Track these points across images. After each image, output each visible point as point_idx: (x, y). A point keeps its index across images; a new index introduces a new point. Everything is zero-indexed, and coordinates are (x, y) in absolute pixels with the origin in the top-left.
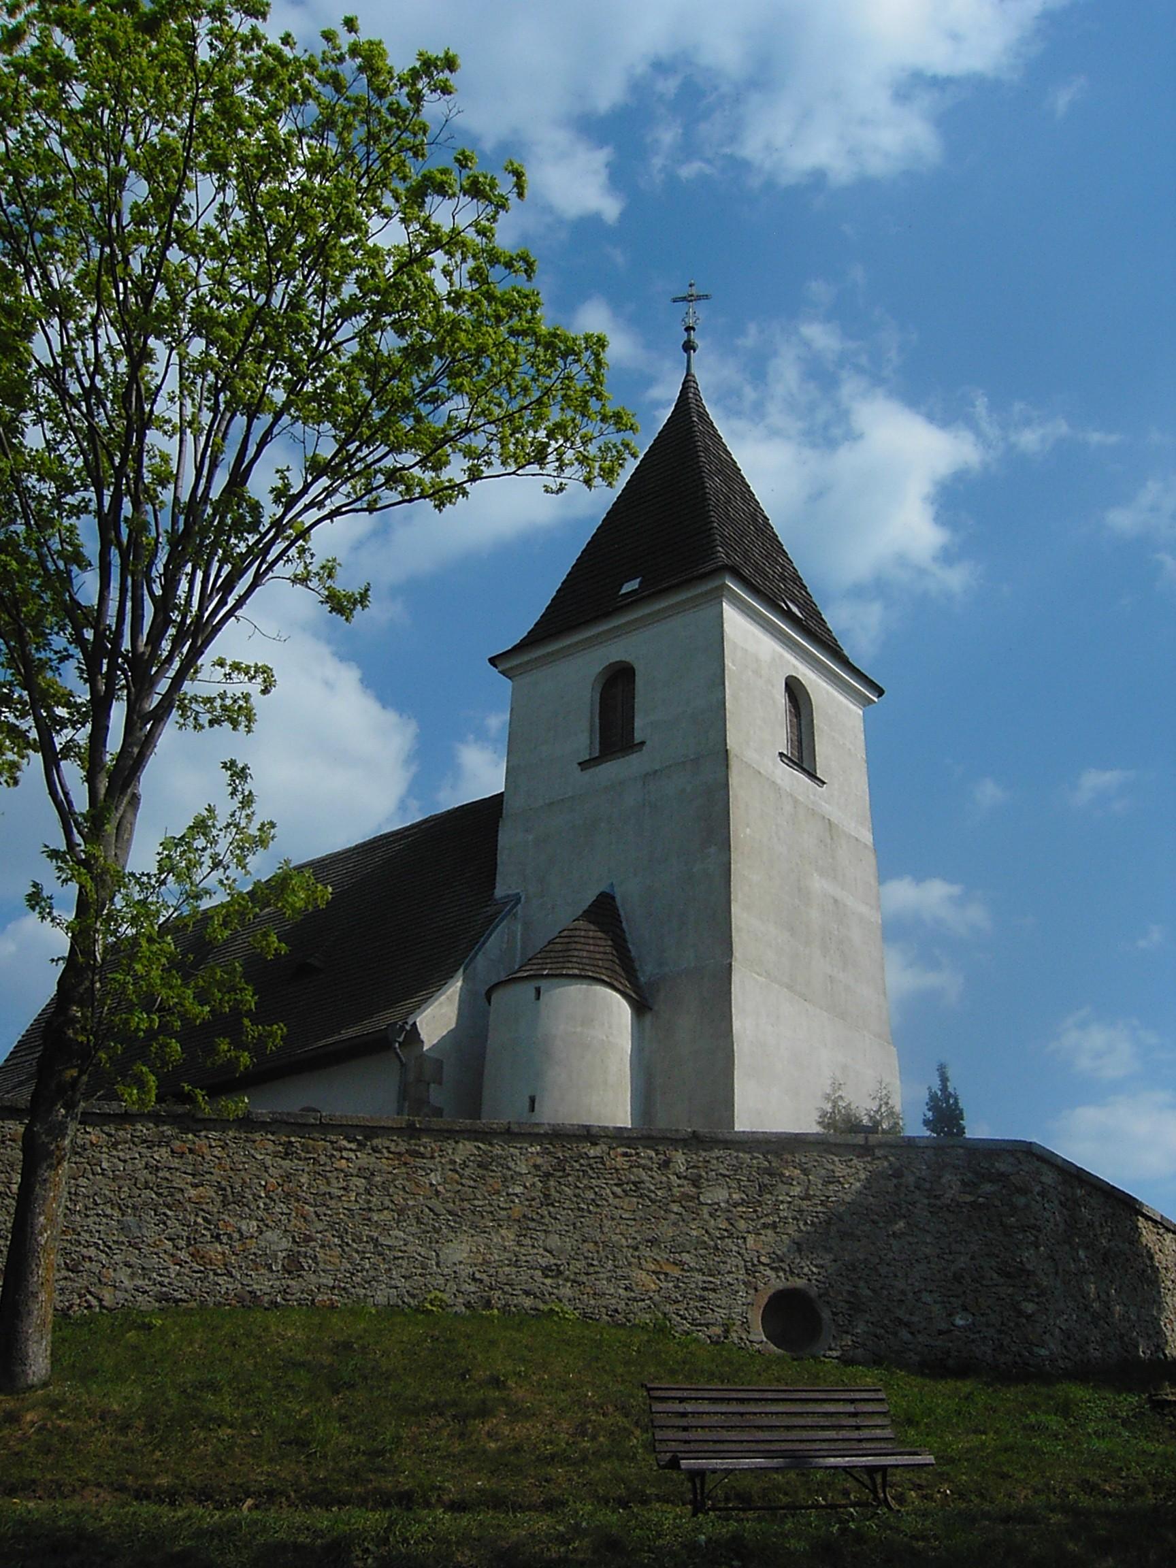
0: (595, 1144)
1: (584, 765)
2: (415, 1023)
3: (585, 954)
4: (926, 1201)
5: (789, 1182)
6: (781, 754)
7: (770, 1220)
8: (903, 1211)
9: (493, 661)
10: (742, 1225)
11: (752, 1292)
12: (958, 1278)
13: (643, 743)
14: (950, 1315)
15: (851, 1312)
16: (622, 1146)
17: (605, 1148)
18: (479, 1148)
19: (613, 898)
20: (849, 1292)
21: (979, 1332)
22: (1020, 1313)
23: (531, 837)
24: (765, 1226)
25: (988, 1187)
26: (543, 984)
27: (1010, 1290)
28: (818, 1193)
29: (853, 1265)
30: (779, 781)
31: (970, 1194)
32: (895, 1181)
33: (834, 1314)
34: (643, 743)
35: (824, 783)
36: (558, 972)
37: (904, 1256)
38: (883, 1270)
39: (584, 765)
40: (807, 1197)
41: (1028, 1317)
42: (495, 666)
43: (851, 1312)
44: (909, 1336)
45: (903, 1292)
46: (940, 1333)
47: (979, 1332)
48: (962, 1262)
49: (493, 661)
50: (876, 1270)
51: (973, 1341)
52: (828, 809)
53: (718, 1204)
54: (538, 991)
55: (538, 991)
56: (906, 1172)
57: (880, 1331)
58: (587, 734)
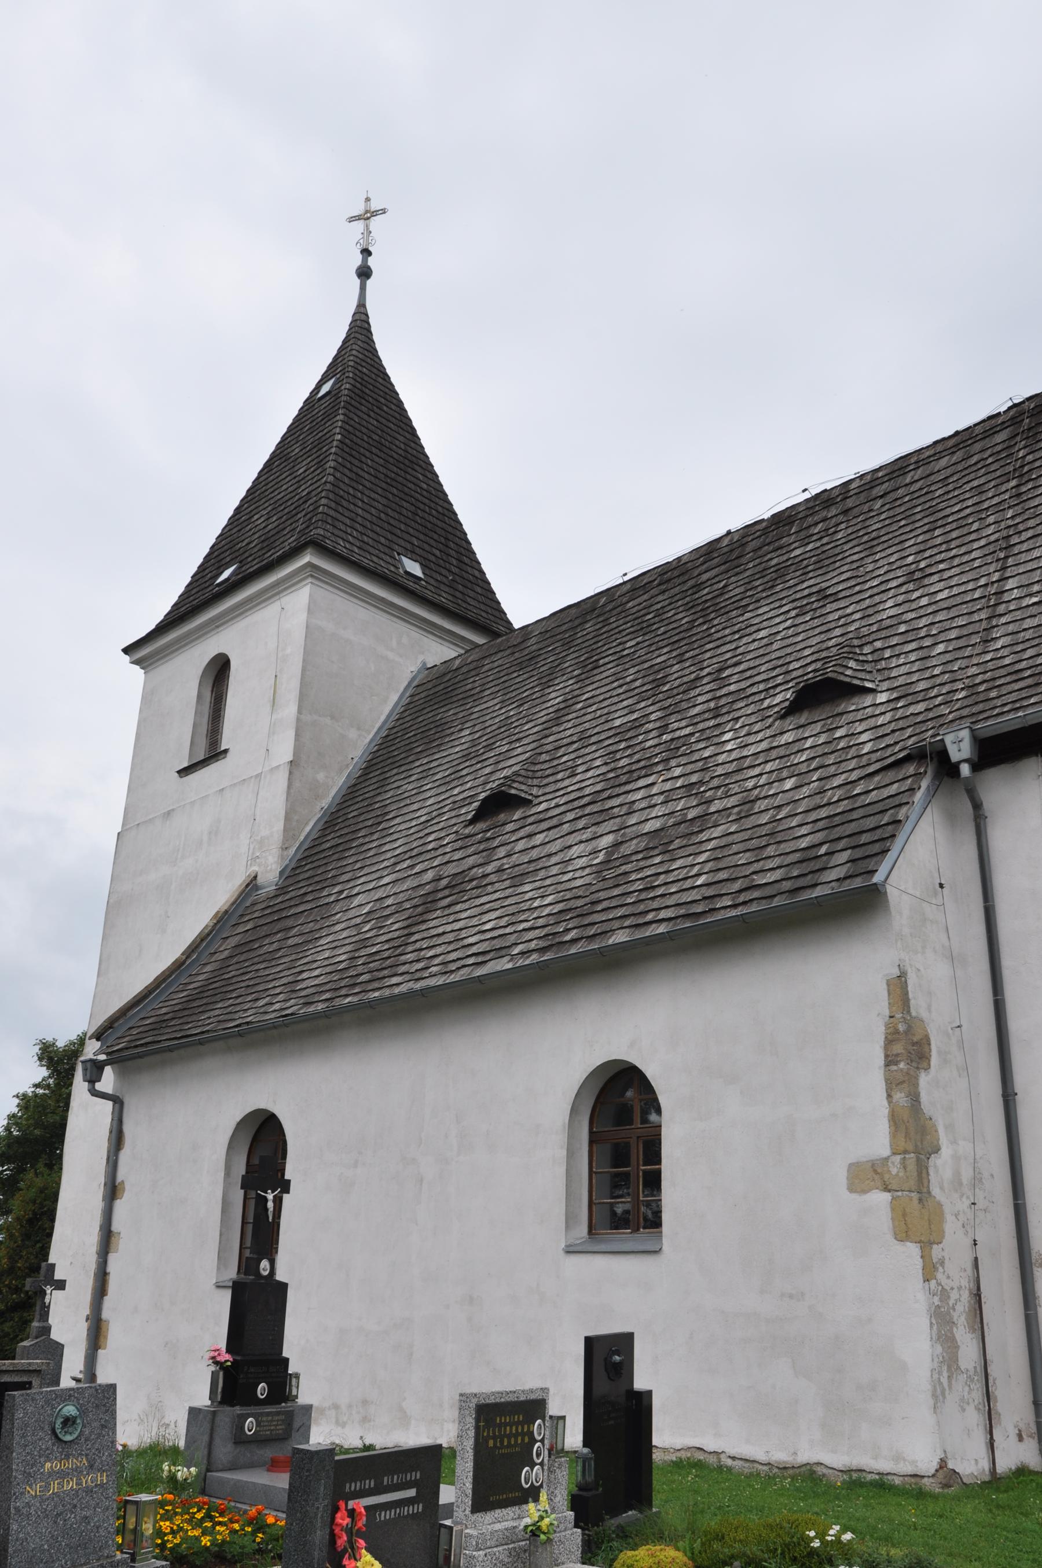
13: (226, 751)
34: (226, 751)
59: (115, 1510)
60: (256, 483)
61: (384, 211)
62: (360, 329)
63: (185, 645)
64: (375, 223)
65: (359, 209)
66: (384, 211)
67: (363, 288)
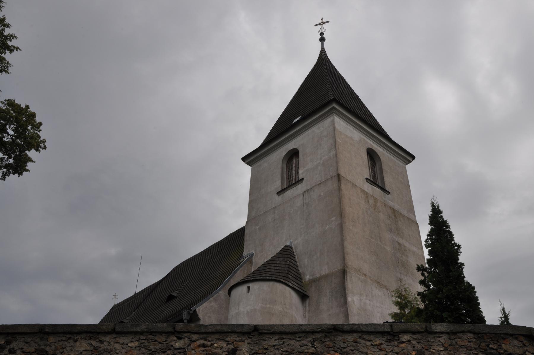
0: (179, 338)
1: (279, 193)
2: (195, 310)
3: (273, 271)
6: (367, 179)
9: (244, 159)
13: (302, 179)
16: (201, 339)
17: (187, 341)
18: (91, 344)
19: (291, 248)
23: (257, 228)
26: (251, 285)
30: (366, 190)
34: (302, 179)
35: (389, 193)
36: (258, 278)
39: (279, 193)
42: (244, 162)
49: (244, 159)
52: (391, 204)
54: (249, 288)
55: (249, 288)
58: (280, 181)
64: (325, 26)
65: (320, 22)
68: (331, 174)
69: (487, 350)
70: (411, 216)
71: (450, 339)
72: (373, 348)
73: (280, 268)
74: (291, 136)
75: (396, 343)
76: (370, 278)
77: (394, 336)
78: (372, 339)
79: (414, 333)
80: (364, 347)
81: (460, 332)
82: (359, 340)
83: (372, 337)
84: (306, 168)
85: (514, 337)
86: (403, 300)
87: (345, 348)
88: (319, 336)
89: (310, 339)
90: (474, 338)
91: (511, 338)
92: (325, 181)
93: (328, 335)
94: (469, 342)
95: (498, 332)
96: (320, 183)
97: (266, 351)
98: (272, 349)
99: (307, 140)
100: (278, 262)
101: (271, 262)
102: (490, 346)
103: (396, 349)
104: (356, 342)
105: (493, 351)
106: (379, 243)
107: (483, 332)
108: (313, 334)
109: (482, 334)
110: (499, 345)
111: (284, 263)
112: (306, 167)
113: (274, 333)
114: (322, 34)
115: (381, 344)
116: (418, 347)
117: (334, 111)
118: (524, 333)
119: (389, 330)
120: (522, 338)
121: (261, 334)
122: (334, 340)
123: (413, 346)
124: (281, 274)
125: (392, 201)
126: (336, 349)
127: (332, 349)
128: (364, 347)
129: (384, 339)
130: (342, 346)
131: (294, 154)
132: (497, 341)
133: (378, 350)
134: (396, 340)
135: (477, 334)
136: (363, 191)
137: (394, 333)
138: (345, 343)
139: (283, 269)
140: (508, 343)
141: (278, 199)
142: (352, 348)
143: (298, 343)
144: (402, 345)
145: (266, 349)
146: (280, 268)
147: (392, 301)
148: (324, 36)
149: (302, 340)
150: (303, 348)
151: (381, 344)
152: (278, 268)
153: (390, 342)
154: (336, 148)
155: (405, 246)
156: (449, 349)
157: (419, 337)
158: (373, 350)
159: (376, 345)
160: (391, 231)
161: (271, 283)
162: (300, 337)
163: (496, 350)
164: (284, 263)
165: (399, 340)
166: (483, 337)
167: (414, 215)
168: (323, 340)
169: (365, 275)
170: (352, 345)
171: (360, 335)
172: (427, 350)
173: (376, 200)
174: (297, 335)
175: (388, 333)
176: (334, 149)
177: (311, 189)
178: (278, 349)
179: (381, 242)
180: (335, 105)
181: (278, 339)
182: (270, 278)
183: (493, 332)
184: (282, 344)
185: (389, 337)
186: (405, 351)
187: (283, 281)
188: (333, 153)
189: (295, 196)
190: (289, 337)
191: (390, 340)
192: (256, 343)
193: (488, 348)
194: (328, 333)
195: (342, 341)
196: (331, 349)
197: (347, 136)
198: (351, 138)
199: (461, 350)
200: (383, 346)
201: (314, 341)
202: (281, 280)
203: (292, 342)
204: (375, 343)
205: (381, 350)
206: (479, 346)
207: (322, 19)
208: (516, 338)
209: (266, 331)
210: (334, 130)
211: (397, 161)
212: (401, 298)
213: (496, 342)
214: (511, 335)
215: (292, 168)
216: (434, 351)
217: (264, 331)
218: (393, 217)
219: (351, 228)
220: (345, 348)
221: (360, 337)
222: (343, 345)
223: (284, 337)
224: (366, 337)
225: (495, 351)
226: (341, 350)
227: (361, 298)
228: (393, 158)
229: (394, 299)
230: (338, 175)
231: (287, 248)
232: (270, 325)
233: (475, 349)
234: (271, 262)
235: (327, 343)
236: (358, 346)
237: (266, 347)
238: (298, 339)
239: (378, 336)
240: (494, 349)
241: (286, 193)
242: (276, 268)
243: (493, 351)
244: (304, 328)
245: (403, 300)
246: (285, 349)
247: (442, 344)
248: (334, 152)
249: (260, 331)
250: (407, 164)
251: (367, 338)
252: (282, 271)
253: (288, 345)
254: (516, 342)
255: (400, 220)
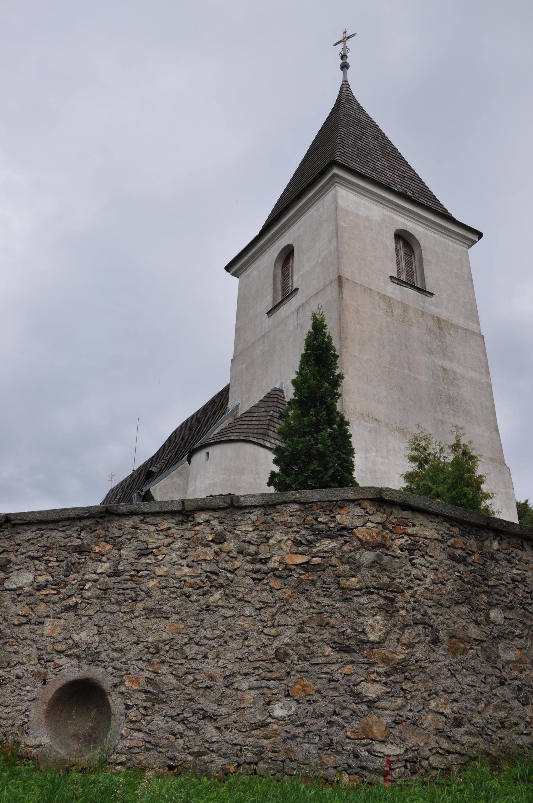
3: (245, 427)
4: (249, 567)
5: (99, 558)
6: (391, 277)
7: (72, 601)
8: (221, 580)
9: (228, 268)
10: (42, 608)
11: (39, 684)
12: (281, 656)
13: (297, 289)
14: (269, 703)
15: (149, 704)
19: (282, 391)
20: (149, 681)
21: (303, 725)
22: (358, 697)
23: (244, 366)
24: (67, 609)
25: (327, 544)
26: (210, 450)
27: (347, 669)
28: (128, 568)
29: (156, 647)
30: (390, 295)
31: (302, 554)
32: (216, 547)
33: (128, 707)
34: (297, 289)
35: (432, 294)
37: (217, 633)
38: (190, 650)
40: (116, 573)
41: (371, 704)
42: (229, 271)
43: (149, 704)
44: (215, 732)
45: (212, 678)
46: (255, 726)
47: (303, 725)
48: (287, 636)
50: (183, 652)
51: (294, 737)
52: (435, 311)
53: (21, 588)
54: (208, 454)
56: (229, 536)
57: (179, 727)
58: (271, 295)
59: (281, 643)
60: (314, 142)
61: (354, 35)
62: (345, 87)
63: (288, 228)
64: (349, 43)
65: (341, 38)
66: (354, 35)
67: (345, 74)
68: (331, 277)
69: (313, 525)
70: (472, 326)
71: (265, 515)
72: (158, 534)
73: (257, 423)
74: (284, 226)
75: (189, 525)
76: (387, 424)
77: (188, 516)
78: (158, 522)
79: (215, 510)
80: (145, 533)
81: (280, 504)
82: (140, 525)
83: (158, 520)
84: (301, 273)
85: (356, 503)
86: (422, 453)
87: (119, 537)
88: (88, 523)
89: (76, 528)
90: (299, 510)
91: (353, 505)
92: (323, 290)
93: (101, 521)
94: (291, 516)
95: (334, 499)
96: (317, 293)
97: (18, 547)
98: (26, 544)
99: (304, 231)
100: (256, 414)
101: (245, 415)
102: (319, 519)
103: (188, 534)
104: (136, 528)
105: (321, 526)
106: (407, 371)
107: (311, 501)
108: (80, 521)
109: (310, 503)
110: (332, 517)
111: (265, 414)
112: (302, 272)
113: (30, 523)
114: (343, 57)
115: (169, 528)
116: (219, 528)
117: (337, 179)
118: (370, 497)
119: (179, 509)
120: (366, 504)
121: (14, 525)
122: (108, 527)
123: (211, 527)
124: (255, 431)
125: (439, 307)
126: (108, 539)
127: (103, 539)
128: (145, 533)
129: (174, 521)
130: (116, 535)
131: (288, 255)
132: (331, 511)
133: (163, 537)
134: (191, 521)
135: (304, 504)
136: (384, 297)
137: (187, 512)
138: (120, 529)
139: (261, 423)
140: (345, 512)
141: (268, 321)
142: (129, 537)
143: (61, 534)
144: (197, 528)
145: (19, 545)
146: (257, 423)
147: (405, 456)
148: (348, 61)
149: (66, 530)
150: (66, 540)
151: (169, 528)
152: (253, 423)
153: (182, 525)
154: (337, 236)
155: (454, 372)
156: (261, 528)
157: (222, 514)
158: (157, 536)
159: (162, 530)
160: (430, 351)
161: (238, 445)
162: (64, 526)
163: (326, 523)
164: (265, 414)
165: (194, 520)
166: (311, 507)
167: (478, 323)
168: (94, 528)
169: (378, 421)
170: (129, 533)
171: (142, 518)
172: (230, 532)
173: (406, 308)
174: (61, 524)
175: (179, 512)
176: (336, 238)
177: (307, 302)
178: (33, 544)
179: (410, 370)
180: (336, 171)
181: (36, 531)
182: (236, 438)
183: (326, 499)
184: (39, 537)
185: (180, 518)
186: (199, 536)
187: (255, 440)
188: (334, 244)
189: (288, 316)
190: (50, 527)
191: (182, 521)
192: (9, 538)
193: (314, 522)
194: (101, 517)
195: (118, 527)
196: (101, 539)
197: (358, 215)
198: (367, 219)
199: (278, 528)
200: (170, 532)
201: (82, 530)
202: (251, 439)
203: (53, 534)
204: (162, 528)
205: (167, 536)
206: (304, 521)
207: (345, 32)
208: (359, 505)
209: (20, 522)
210: (336, 210)
211: (451, 243)
212: (419, 450)
213: (328, 513)
214: (353, 501)
215: (289, 274)
216: (239, 532)
217: (17, 521)
218: (437, 331)
219: (357, 354)
220: (119, 537)
221: (142, 521)
222: (117, 533)
223: (44, 527)
224: (150, 520)
225: (324, 526)
226: (115, 540)
227: (368, 455)
228: (442, 239)
229: (409, 452)
230: (340, 278)
231: (274, 392)
232: (25, 513)
233: (298, 525)
234: (245, 415)
235: (98, 532)
236: (137, 533)
237: (19, 542)
238: (61, 529)
239: (166, 517)
240: (323, 523)
241: (278, 312)
242: (250, 423)
243: (321, 526)
244: (67, 514)
245: (422, 453)
246: (43, 543)
247: (253, 523)
248: (335, 243)
249: (13, 522)
250: (470, 247)
251: (151, 522)
252: (259, 427)
253: (48, 537)
254: (358, 511)
255: (450, 334)
